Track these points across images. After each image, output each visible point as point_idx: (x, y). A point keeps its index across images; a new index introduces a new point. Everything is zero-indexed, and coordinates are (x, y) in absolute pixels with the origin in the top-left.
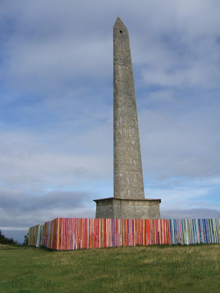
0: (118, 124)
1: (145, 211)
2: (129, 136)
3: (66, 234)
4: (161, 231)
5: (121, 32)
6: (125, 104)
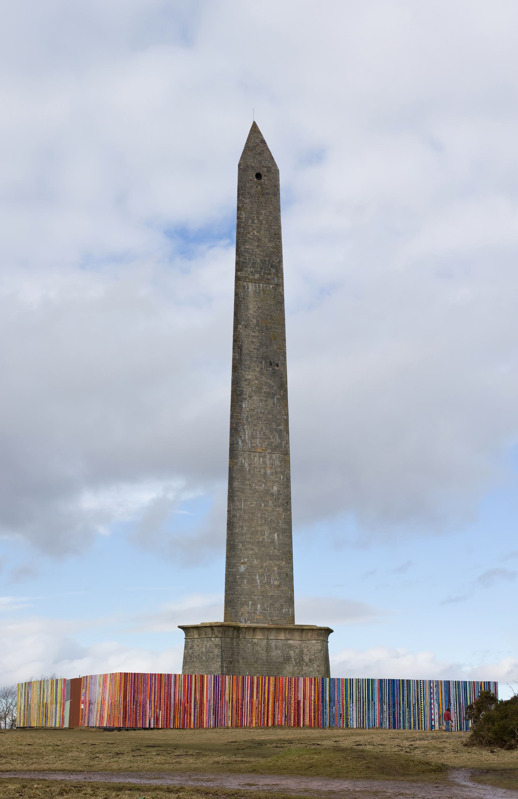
0: (240, 443)
1: (292, 653)
2: (265, 473)
3: (135, 701)
4: (304, 699)
5: (259, 176)
6: (259, 389)
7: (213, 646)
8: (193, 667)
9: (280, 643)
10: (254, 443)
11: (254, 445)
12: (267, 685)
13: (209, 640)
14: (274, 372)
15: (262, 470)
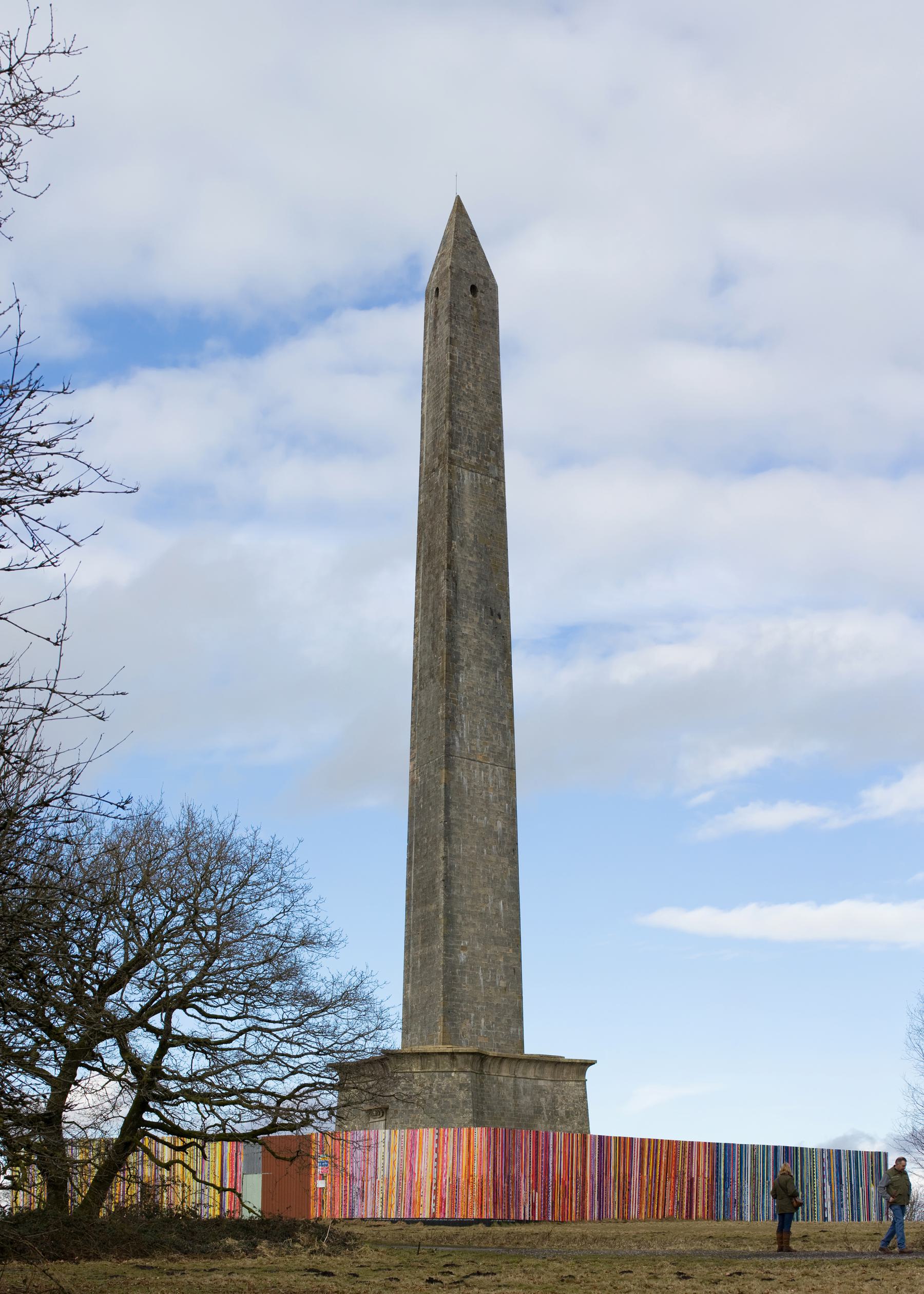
3: (508, 1177)
4: (698, 1176)
5: (474, 289)
7: (455, 1086)
8: (413, 1121)
9: (530, 1084)
10: (473, 745)
11: (473, 748)
12: (659, 1152)
13: (446, 1076)
14: (496, 627)
15: (484, 792)
